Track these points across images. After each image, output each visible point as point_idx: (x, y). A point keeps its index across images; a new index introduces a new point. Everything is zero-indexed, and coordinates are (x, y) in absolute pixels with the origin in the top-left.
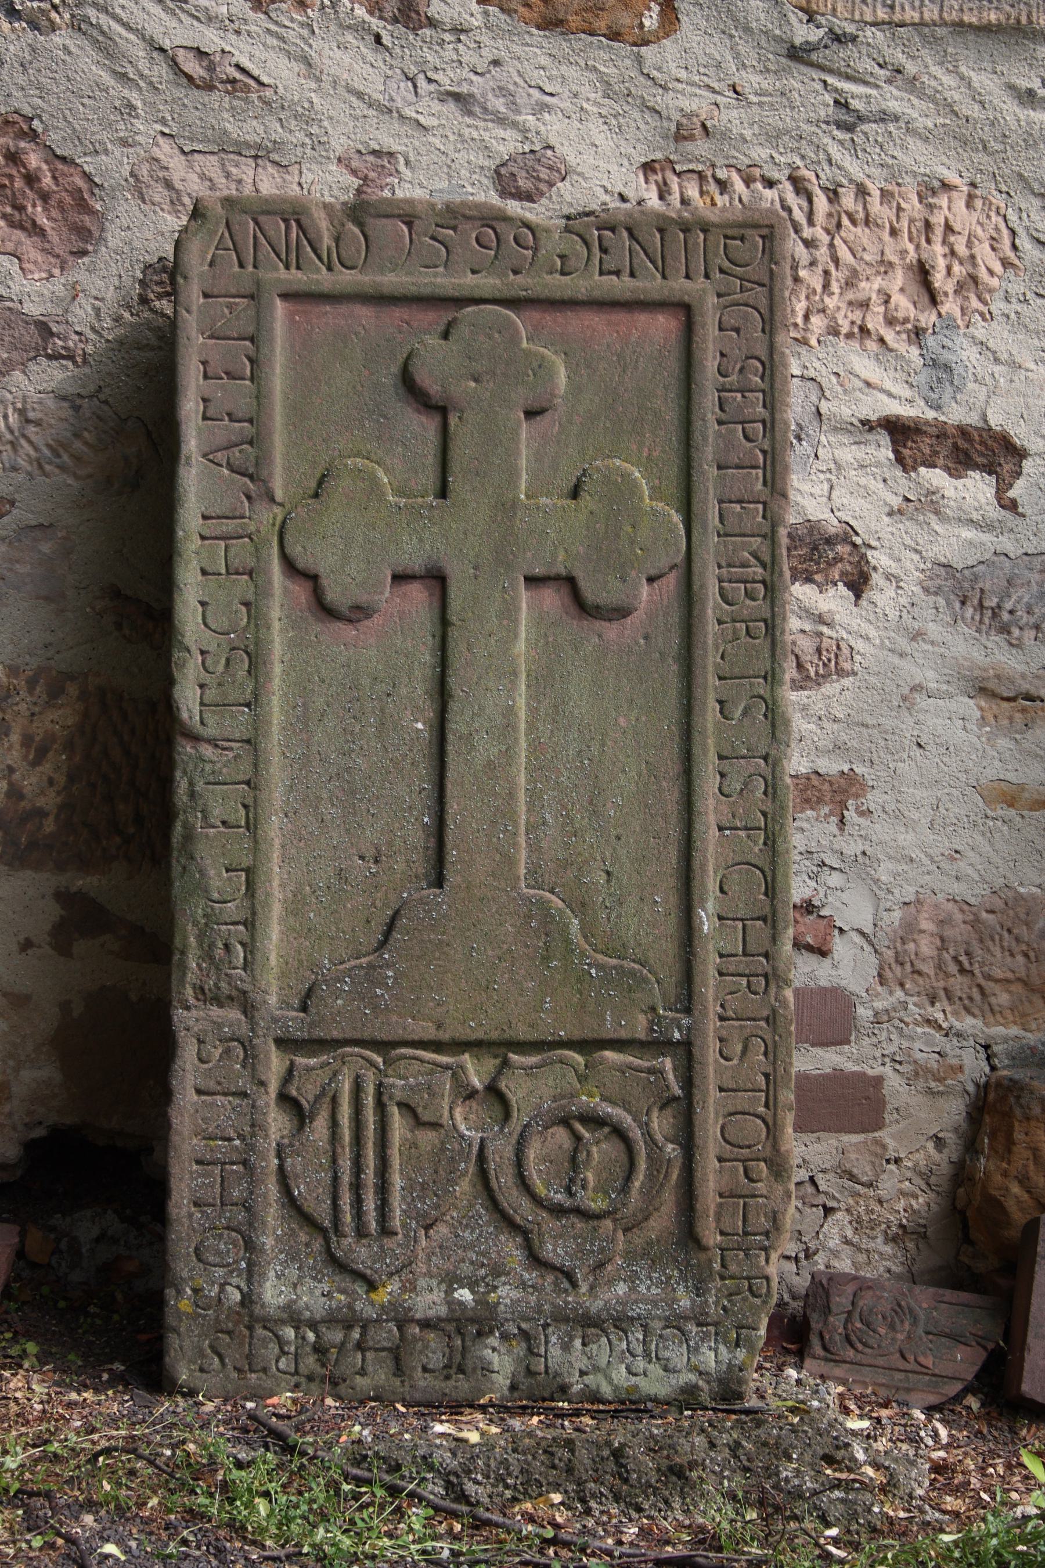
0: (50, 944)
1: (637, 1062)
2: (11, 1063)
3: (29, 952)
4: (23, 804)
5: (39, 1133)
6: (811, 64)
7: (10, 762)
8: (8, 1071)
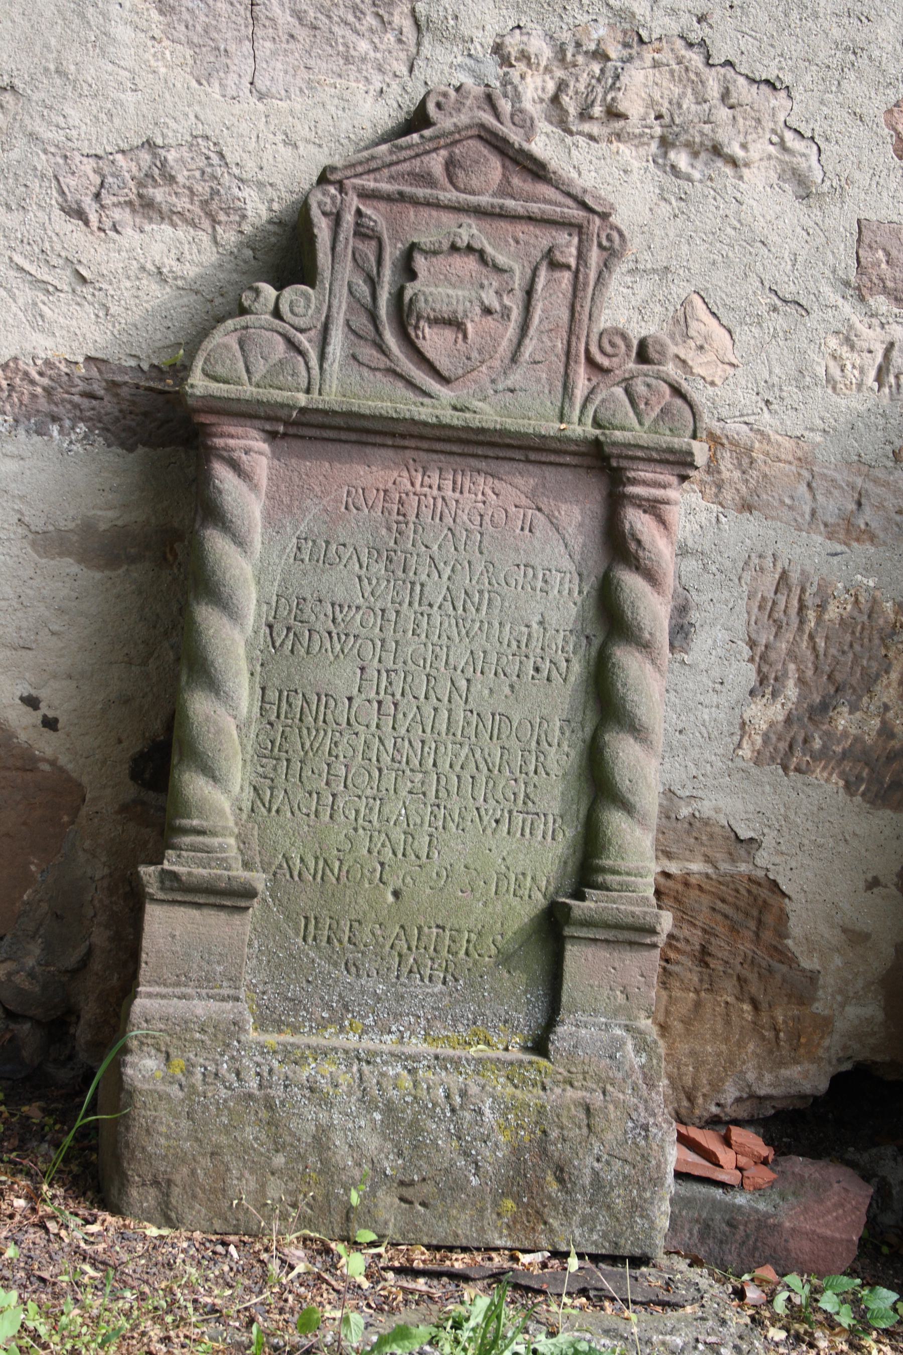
0: (896, 885)
1: (566, 210)
2: (839, 998)
3: (875, 890)
4: (893, 743)
5: (847, 1066)
6: (563, 398)
7: (885, 700)
8: (835, 1006)
